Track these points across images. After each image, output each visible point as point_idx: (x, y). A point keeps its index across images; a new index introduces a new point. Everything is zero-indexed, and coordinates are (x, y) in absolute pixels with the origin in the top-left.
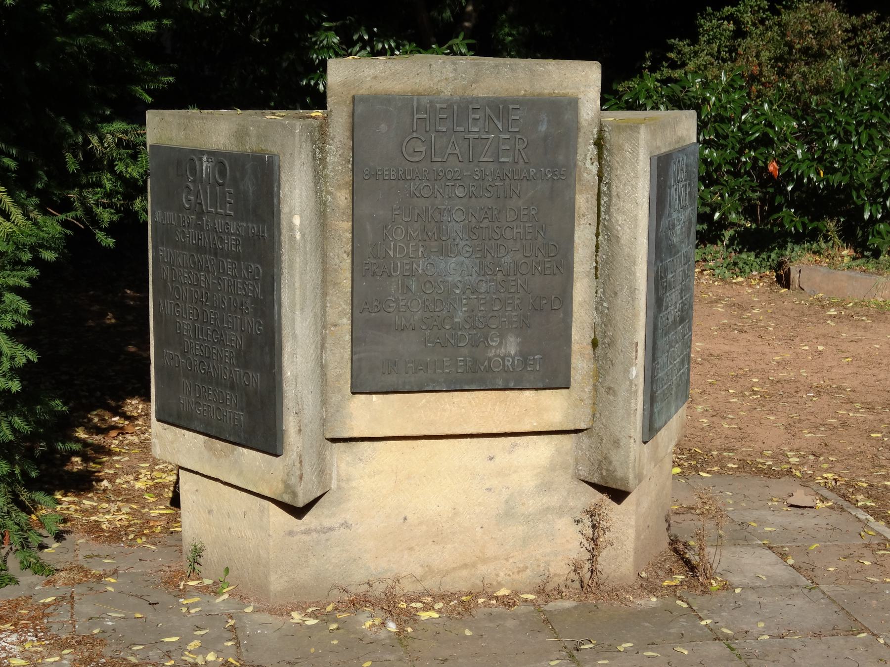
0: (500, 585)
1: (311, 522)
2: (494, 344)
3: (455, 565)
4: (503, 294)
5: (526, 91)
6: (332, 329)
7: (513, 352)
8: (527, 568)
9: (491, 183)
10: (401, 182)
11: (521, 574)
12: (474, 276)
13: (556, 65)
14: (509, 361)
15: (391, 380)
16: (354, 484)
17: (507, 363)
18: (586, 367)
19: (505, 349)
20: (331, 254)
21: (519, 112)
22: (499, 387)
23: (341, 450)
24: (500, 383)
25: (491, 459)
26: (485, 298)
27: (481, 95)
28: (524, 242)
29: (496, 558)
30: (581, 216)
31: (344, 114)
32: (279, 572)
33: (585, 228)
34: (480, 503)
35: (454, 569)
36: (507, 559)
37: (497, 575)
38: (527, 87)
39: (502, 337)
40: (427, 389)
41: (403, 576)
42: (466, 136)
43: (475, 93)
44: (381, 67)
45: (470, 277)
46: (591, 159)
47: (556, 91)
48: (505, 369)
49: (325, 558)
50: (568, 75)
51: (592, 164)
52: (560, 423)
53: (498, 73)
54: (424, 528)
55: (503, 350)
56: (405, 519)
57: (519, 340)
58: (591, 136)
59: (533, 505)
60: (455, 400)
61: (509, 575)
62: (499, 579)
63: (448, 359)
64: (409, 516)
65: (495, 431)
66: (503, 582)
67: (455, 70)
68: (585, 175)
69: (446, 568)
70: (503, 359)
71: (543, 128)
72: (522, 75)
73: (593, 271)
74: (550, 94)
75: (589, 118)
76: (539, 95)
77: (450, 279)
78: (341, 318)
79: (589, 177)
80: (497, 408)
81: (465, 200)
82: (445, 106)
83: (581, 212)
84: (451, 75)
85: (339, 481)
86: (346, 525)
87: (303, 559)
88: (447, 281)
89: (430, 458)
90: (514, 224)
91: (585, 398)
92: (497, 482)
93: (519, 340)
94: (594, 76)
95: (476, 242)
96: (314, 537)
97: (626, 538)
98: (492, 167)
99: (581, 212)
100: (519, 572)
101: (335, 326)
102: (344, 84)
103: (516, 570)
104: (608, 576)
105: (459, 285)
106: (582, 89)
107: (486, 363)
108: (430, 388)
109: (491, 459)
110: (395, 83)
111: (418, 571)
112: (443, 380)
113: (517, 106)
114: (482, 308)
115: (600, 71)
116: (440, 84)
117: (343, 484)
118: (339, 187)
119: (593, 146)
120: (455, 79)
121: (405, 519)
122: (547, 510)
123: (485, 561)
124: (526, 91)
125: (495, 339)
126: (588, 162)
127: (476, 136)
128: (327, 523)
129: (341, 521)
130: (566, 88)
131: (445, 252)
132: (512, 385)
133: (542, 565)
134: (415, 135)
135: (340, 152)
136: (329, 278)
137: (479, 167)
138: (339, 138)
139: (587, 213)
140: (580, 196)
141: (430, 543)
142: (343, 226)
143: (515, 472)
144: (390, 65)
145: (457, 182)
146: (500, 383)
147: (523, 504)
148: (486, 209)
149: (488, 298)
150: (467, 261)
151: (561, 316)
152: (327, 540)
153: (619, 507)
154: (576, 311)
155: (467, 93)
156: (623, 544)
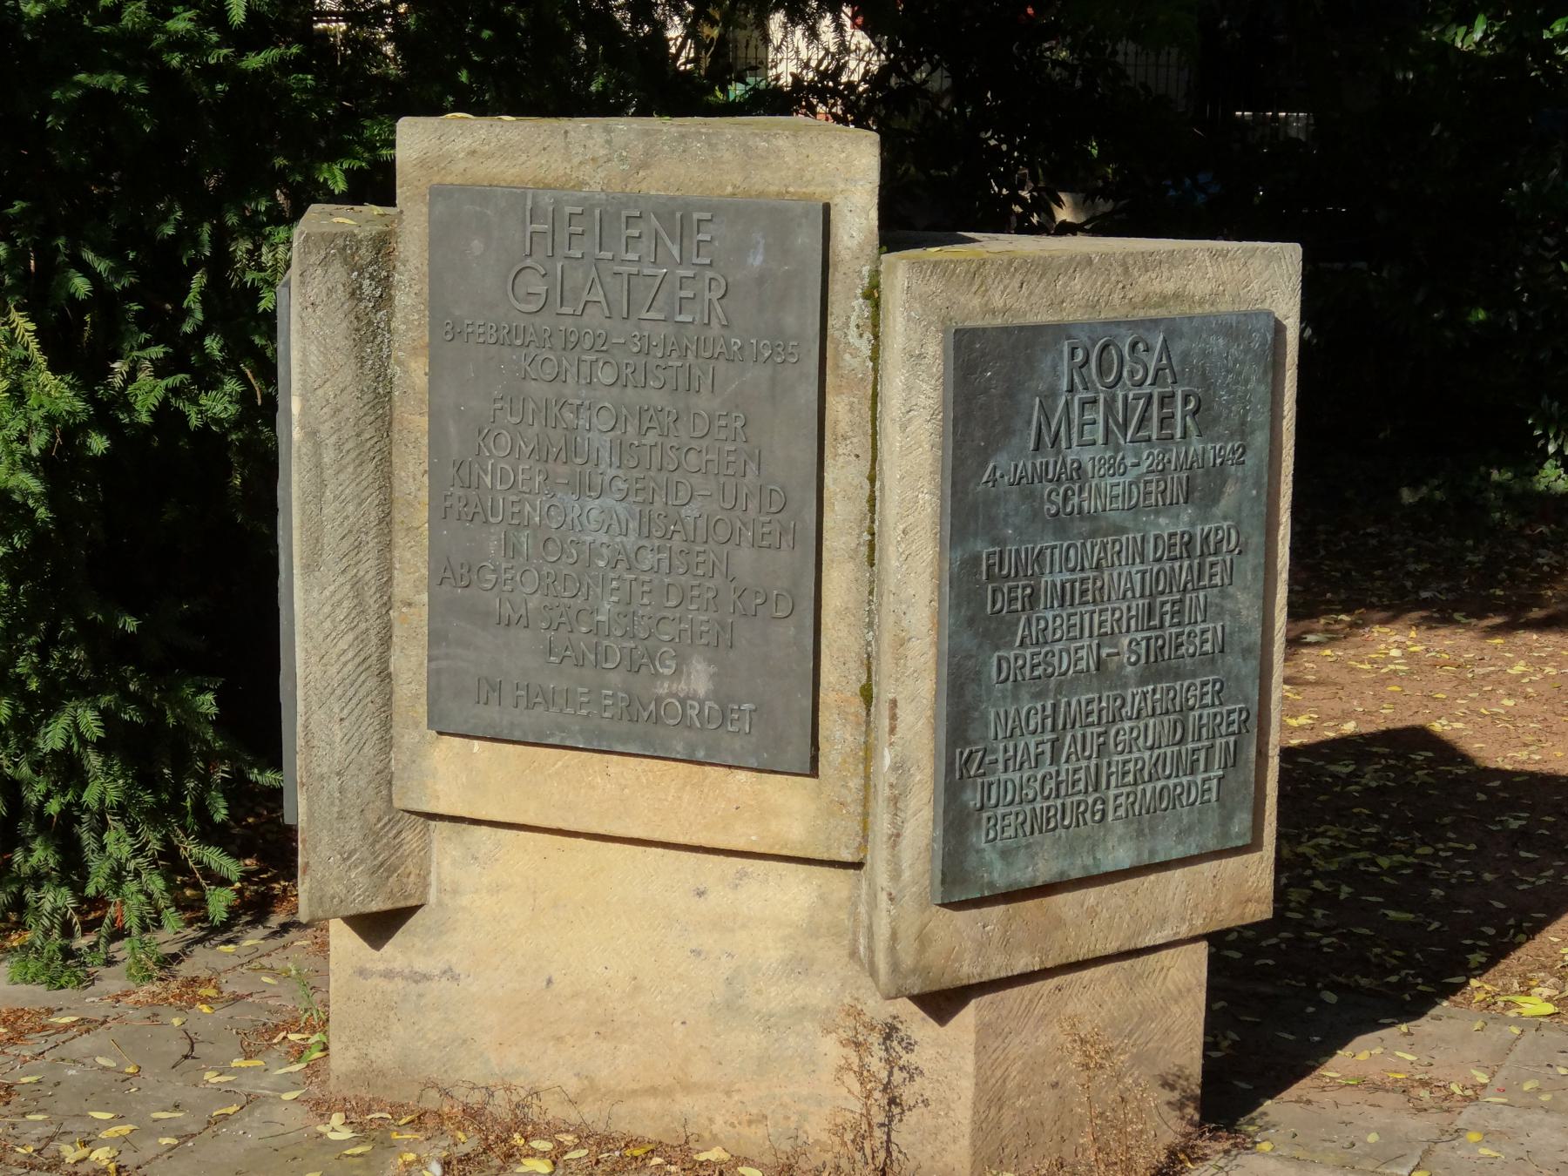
0: (715, 1140)
1: (395, 959)
2: (666, 671)
3: (635, 1086)
4: (683, 578)
5: (734, 186)
6: (404, 610)
7: (702, 692)
8: (765, 1117)
9: (660, 362)
10: (506, 351)
11: (753, 1126)
12: (632, 537)
13: (791, 138)
14: (692, 707)
15: (492, 715)
16: (464, 901)
17: (689, 712)
18: (851, 739)
19: (688, 684)
20: (403, 474)
21: (711, 226)
22: (678, 756)
23: (444, 835)
24: (679, 748)
25: (700, 894)
26: (651, 581)
27: (653, 192)
28: (722, 480)
29: (709, 1087)
30: (840, 439)
31: (422, 219)
32: (344, 1039)
33: (849, 463)
34: (680, 975)
35: (634, 1092)
36: (728, 1093)
37: (711, 1120)
38: (737, 178)
39: (682, 661)
40: (550, 741)
41: (544, 1086)
42: (617, 269)
43: (644, 187)
44: (483, 134)
45: (625, 539)
46: (858, 326)
47: (791, 189)
48: (684, 723)
49: (417, 1028)
50: (814, 157)
51: (861, 336)
52: (801, 843)
53: (684, 151)
54: (582, 1004)
55: (683, 685)
56: (549, 981)
57: (712, 669)
58: (858, 281)
59: (778, 996)
60: (611, 770)
61: (733, 1125)
62: (715, 1128)
63: (586, 690)
64: (556, 977)
65: (681, 840)
66: (721, 1136)
67: (609, 142)
68: (847, 357)
69: (620, 1088)
70: (683, 702)
71: (756, 260)
72: (727, 156)
73: (864, 550)
74: (779, 195)
75: (853, 244)
76: (761, 194)
77: (589, 539)
78: (418, 592)
79: (855, 363)
80: (686, 797)
81: (615, 391)
82: (579, 210)
83: (840, 431)
84: (602, 152)
85: (440, 891)
86: (450, 973)
87: (381, 1022)
88: (584, 542)
89: (593, 874)
90: (705, 443)
91: (849, 800)
92: (711, 941)
93: (712, 669)
94: (864, 161)
95: (636, 473)
96: (400, 986)
97: (956, 1097)
98: (664, 330)
99: (840, 431)
100: (750, 1123)
101: (410, 605)
102: (422, 163)
103: (745, 1118)
104: (919, 1167)
105: (604, 551)
106: (841, 186)
107: (652, 707)
108: (556, 741)
109: (700, 894)
110: (506, 163)
111: (573, 1086)
112: (577, 728)
113: (707, 216)
114: (645, 601)
115: (876, 151)
116: (582, 168)
117: (446, 899)
118: (415, 352)
119: (861, 300)
120: (609, 160)
121: (549, 981)
122: (802, 1011)
123: (688, 1088)
124: (734, 186)
125: (668, 662)
126: (853, 331)
127: (634, 270)
128: (421, 965)
129: (442, 966)
130: (809, 183)
131: (582, 487)
132: (700, 755)
133: (794, 1118)
134: (529, 262)
135: (416, 288)
136: (398, 516)
137: (640, 329)
138: (414, 262)
139: (850, 434)
140: (838, 399)
141: (593, 1035)
142: (414, 422)
143: (744, 926)
144: (498, 130)
145: (602, 355)
146: (679, 749)
147: (759, 992)
148: (652, 411)
149: (656, 582)
150: (620, 508)
151: (792, 631)
152: (420, 996)
153: (942, 1030)
154: (830, 625)
155: (629, 187)
156: (949, 1106)
